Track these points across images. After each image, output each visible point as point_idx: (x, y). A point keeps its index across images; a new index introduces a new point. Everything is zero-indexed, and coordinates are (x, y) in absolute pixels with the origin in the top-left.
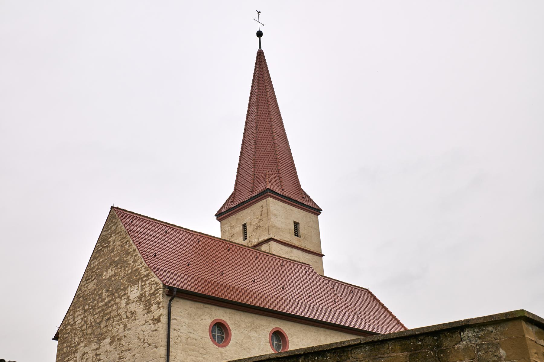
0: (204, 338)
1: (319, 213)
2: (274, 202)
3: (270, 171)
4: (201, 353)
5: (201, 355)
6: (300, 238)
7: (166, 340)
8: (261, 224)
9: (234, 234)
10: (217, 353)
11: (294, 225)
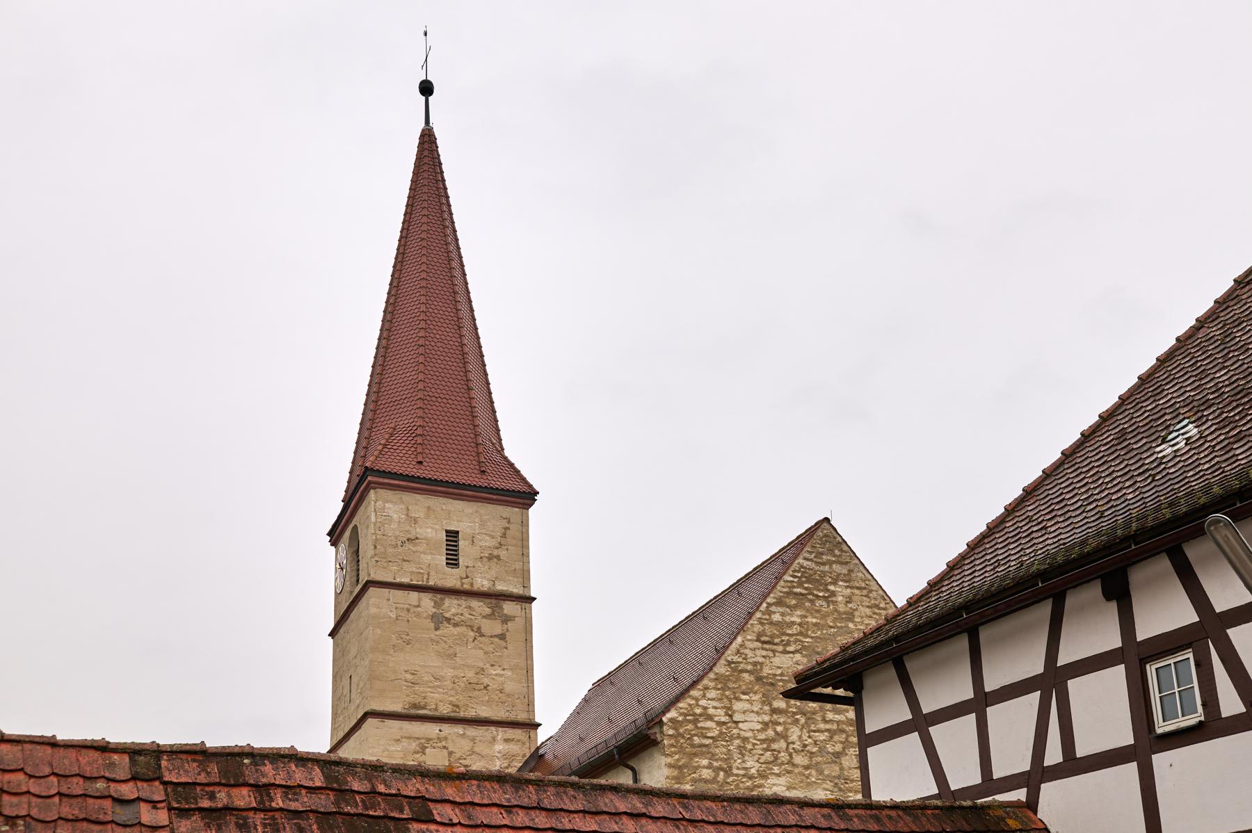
8: (503, 553)
9: (417, 538)
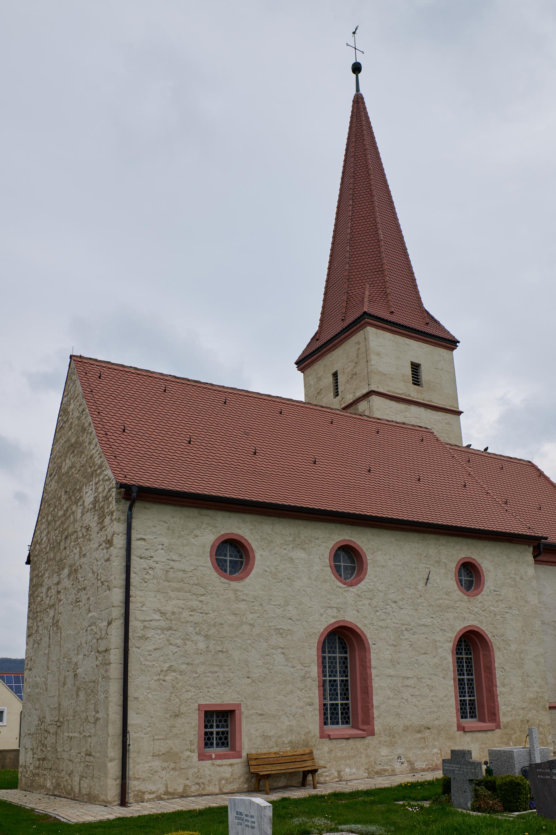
0: (200, 568)
1: (455, 347)
2: (376, 334)
4: (194, 594)
6: (422, 387)
7: (124, 576)
9: (321, 390)
10: (227, 591)
11: (412, 368)
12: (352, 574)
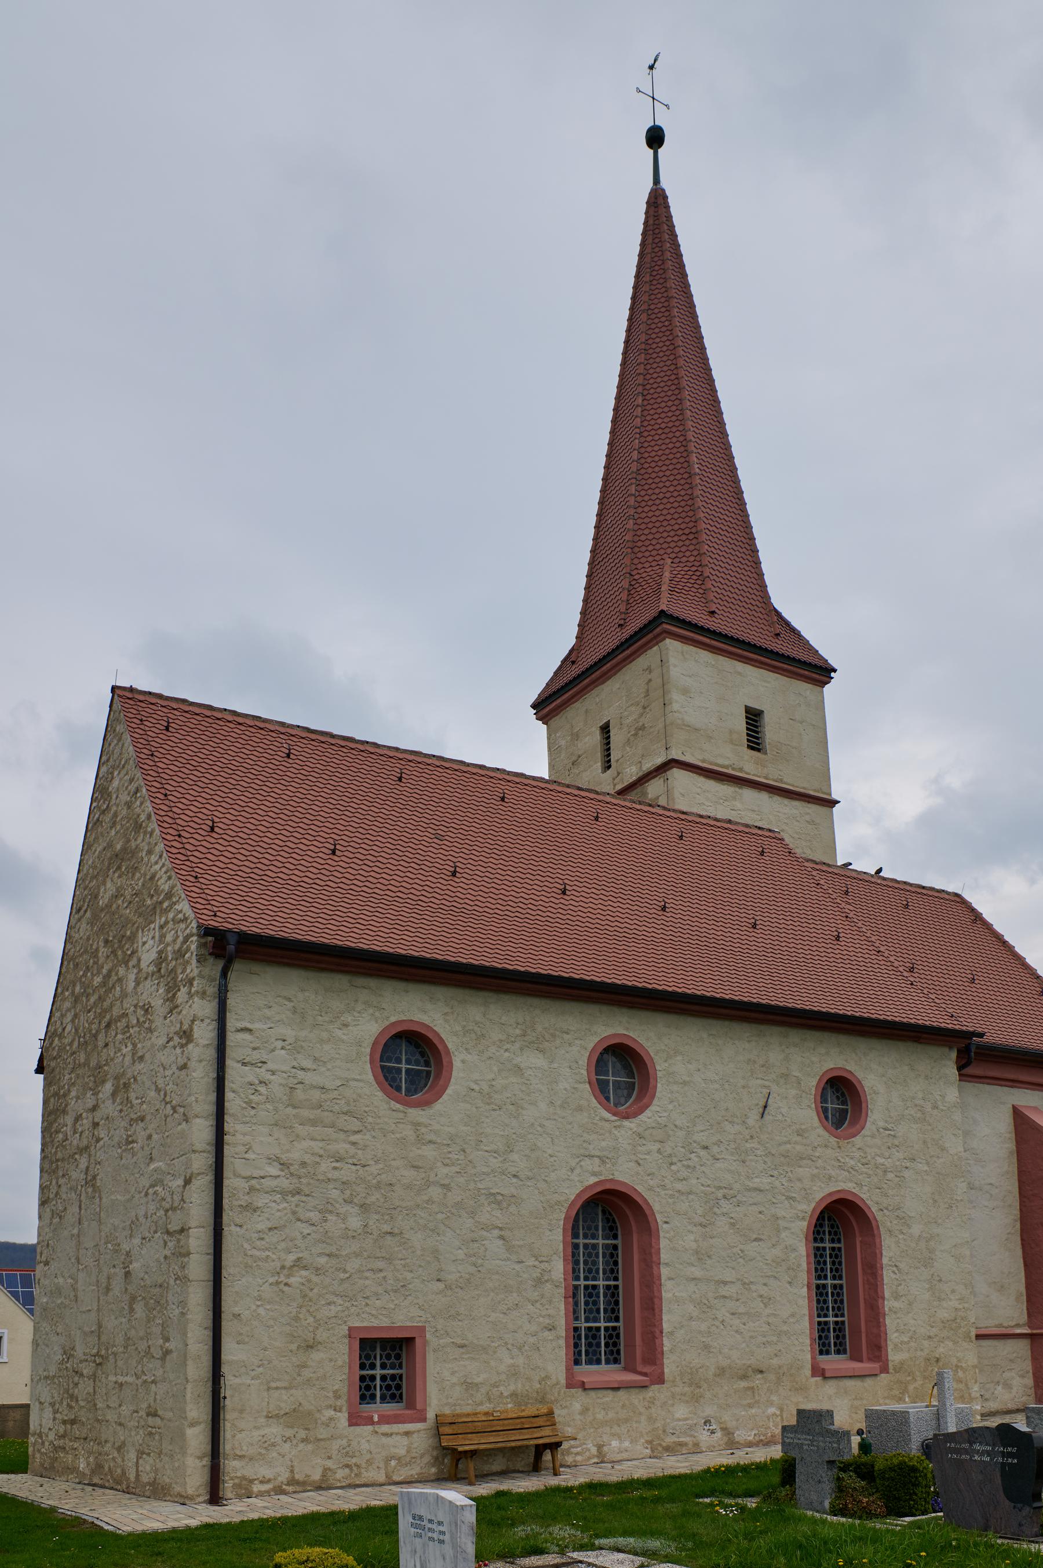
2: (682, 652)
3: (677, 560)
4: (341, 1130)
5: (342, 1136)
6: (766, 753)
9: (579, 757)
11: (747, 717)
12: (629, 1096)
